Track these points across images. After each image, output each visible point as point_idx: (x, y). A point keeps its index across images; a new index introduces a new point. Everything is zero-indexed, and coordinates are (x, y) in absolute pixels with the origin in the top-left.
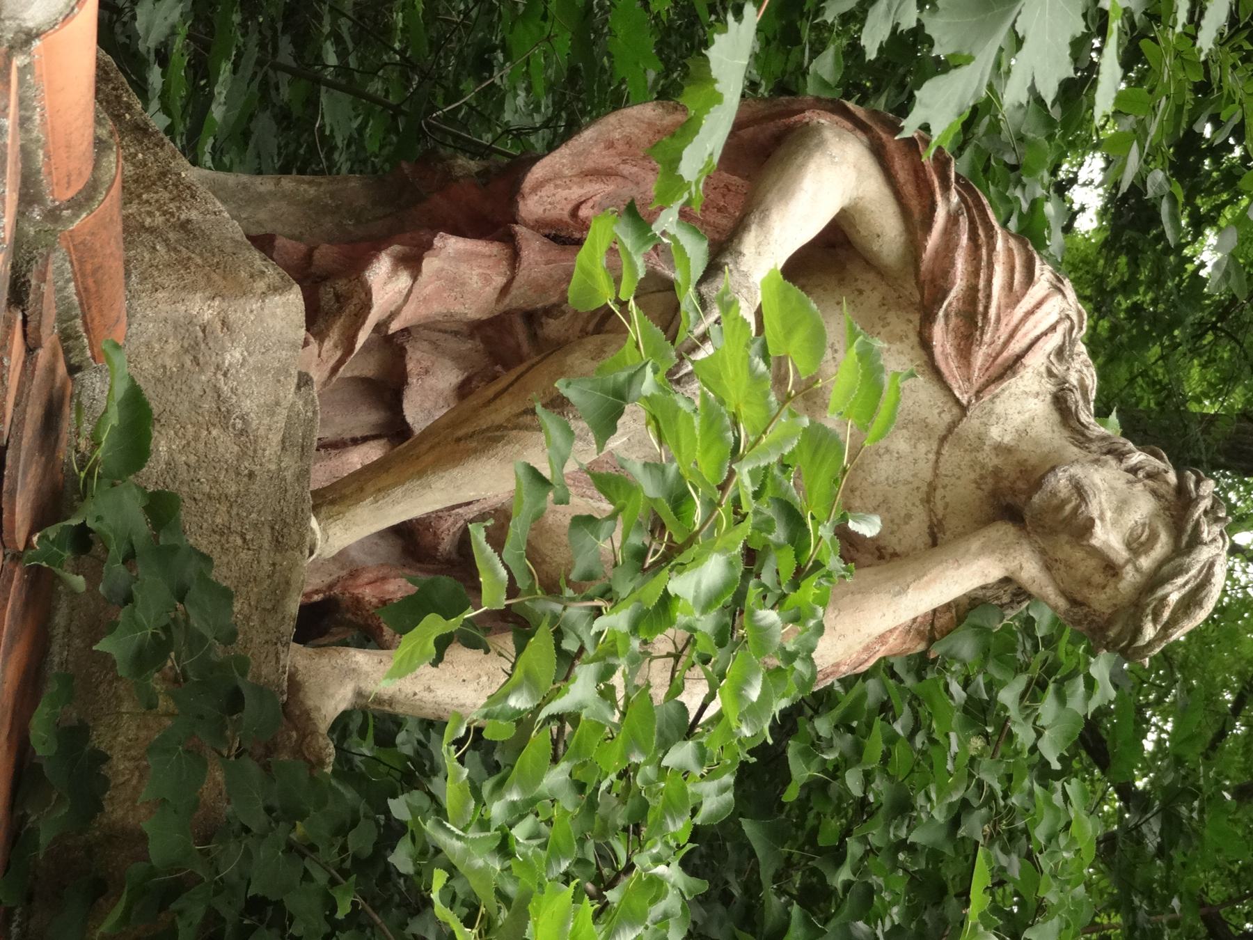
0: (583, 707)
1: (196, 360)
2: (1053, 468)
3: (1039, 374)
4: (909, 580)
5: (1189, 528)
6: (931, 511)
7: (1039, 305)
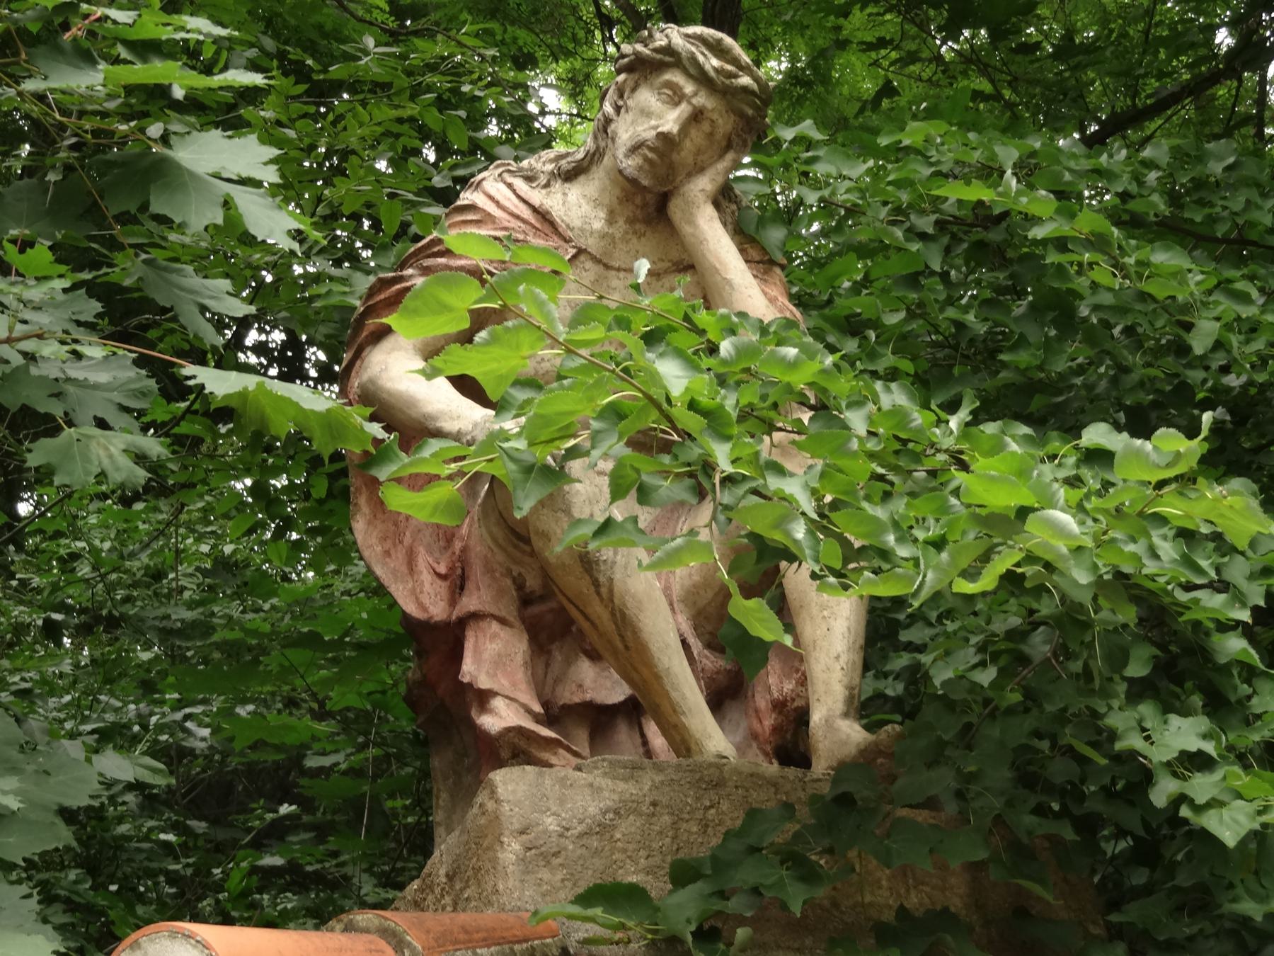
0: (807, 485)
1: (556, 854)
2: (620, 172)
3: (548, 194)
4: (719, 279)
5: (658, 56)
6: (666, 272)
7: (491, 198)
